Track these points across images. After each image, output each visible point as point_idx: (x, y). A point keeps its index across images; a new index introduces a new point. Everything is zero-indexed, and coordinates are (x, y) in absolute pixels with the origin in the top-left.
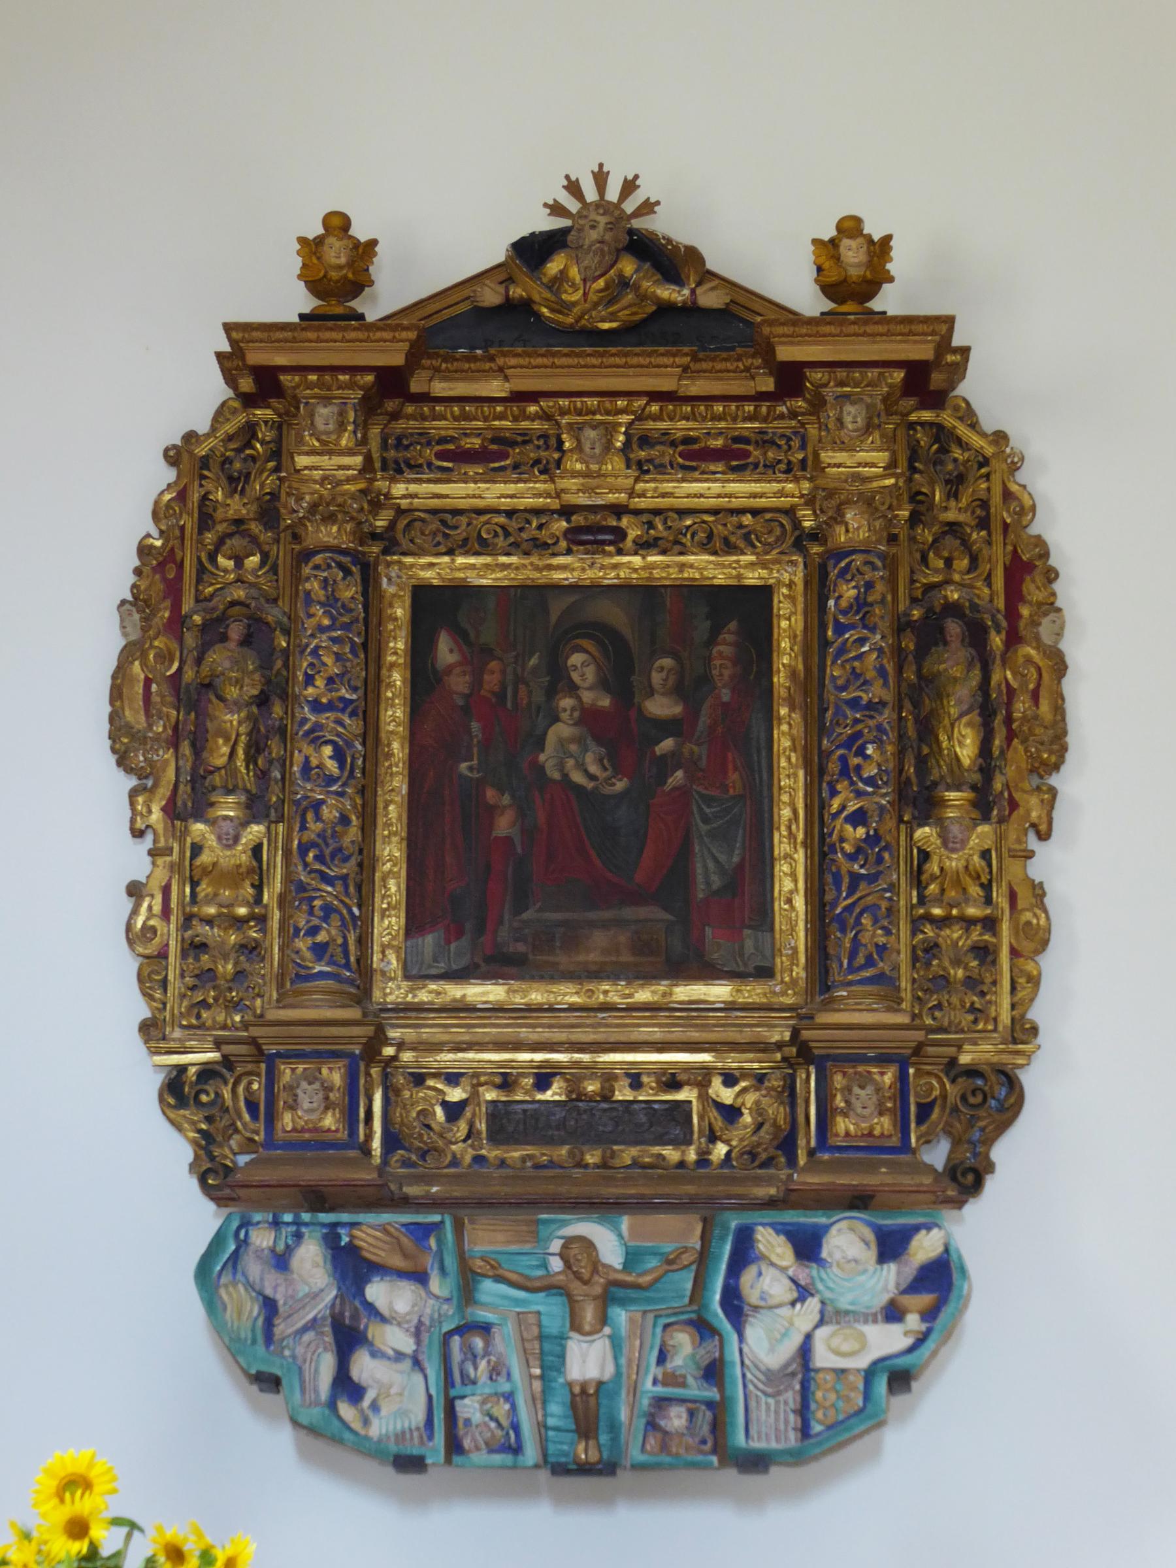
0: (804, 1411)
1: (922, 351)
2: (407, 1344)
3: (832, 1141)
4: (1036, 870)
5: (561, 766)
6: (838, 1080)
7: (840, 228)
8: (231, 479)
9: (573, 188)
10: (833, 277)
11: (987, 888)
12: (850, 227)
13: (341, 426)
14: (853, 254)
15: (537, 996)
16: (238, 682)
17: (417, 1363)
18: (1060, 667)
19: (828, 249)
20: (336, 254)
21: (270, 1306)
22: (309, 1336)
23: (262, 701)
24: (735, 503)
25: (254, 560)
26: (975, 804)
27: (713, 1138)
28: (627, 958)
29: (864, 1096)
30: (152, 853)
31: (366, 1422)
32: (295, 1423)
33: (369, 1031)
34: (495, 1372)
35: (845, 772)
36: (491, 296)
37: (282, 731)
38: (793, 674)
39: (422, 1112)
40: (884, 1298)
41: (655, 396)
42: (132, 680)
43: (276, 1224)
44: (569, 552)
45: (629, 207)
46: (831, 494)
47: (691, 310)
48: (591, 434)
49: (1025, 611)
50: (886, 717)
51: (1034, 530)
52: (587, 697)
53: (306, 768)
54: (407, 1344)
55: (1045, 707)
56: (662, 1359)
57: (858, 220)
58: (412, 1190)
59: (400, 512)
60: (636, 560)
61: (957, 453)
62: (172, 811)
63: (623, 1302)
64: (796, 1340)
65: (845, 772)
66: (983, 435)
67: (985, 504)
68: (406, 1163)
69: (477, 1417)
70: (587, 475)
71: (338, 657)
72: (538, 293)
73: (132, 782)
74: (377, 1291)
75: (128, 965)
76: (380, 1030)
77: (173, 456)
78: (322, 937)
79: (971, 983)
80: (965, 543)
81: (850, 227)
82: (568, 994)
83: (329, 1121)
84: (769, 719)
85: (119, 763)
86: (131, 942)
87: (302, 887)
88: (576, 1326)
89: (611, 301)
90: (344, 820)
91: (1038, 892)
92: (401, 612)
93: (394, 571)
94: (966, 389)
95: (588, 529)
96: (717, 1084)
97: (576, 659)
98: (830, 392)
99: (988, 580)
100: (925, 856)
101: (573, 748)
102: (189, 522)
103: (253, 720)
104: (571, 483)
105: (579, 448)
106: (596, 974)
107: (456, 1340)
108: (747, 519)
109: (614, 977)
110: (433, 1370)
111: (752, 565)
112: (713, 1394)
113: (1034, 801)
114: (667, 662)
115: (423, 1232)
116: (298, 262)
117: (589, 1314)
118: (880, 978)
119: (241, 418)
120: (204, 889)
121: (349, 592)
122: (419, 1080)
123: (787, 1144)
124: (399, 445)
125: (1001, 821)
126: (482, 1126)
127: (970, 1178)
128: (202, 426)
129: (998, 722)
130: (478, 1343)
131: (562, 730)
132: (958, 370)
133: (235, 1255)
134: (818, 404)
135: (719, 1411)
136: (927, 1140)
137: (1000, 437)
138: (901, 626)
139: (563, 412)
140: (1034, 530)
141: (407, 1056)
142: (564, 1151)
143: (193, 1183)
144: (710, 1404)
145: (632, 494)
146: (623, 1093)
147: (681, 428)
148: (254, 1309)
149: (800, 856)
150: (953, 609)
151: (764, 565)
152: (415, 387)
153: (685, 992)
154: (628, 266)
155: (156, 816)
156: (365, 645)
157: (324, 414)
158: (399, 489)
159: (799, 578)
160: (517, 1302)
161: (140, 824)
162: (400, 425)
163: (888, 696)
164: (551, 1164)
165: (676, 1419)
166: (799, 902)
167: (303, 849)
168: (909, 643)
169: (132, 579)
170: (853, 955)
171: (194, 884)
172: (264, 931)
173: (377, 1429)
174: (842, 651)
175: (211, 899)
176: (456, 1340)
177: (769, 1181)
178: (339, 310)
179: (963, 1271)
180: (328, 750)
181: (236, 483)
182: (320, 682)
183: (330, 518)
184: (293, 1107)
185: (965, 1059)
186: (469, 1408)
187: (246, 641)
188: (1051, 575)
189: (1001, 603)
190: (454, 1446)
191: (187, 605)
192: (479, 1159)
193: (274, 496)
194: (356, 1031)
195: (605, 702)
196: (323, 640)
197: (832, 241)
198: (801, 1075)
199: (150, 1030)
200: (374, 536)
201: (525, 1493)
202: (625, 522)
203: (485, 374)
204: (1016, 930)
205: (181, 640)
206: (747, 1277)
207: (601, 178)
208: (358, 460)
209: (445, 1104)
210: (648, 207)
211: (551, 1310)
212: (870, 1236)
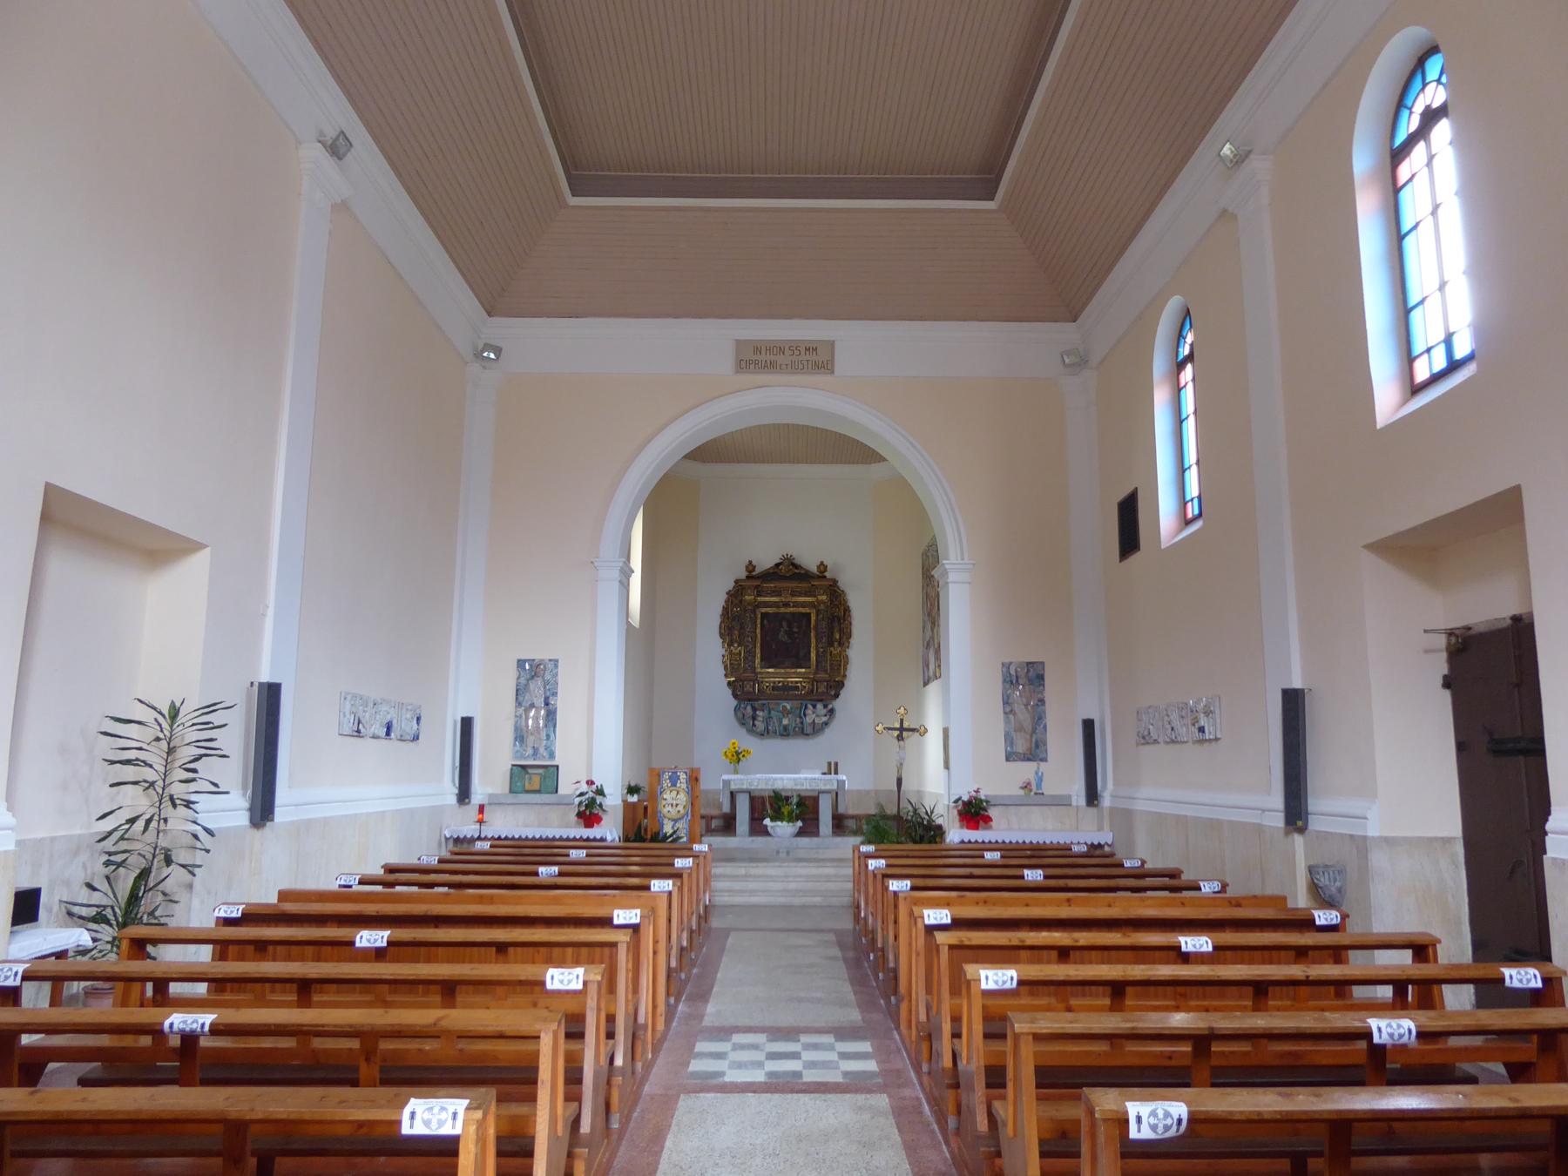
18: (851, 623)
36: (771, 571)
47: (799, 573)
77: (727, 593)
82: (783, 671)
106: (788, 668)
121: (752, 616)
123: (812, 691)
135: (803, 729)
153: (799, 670)
157: (749, 591)
165: (797, 729)
181: (736, 598)
186: (770, 728)
188: (850, 611)
190: (768, 733)
199: (726, 676)
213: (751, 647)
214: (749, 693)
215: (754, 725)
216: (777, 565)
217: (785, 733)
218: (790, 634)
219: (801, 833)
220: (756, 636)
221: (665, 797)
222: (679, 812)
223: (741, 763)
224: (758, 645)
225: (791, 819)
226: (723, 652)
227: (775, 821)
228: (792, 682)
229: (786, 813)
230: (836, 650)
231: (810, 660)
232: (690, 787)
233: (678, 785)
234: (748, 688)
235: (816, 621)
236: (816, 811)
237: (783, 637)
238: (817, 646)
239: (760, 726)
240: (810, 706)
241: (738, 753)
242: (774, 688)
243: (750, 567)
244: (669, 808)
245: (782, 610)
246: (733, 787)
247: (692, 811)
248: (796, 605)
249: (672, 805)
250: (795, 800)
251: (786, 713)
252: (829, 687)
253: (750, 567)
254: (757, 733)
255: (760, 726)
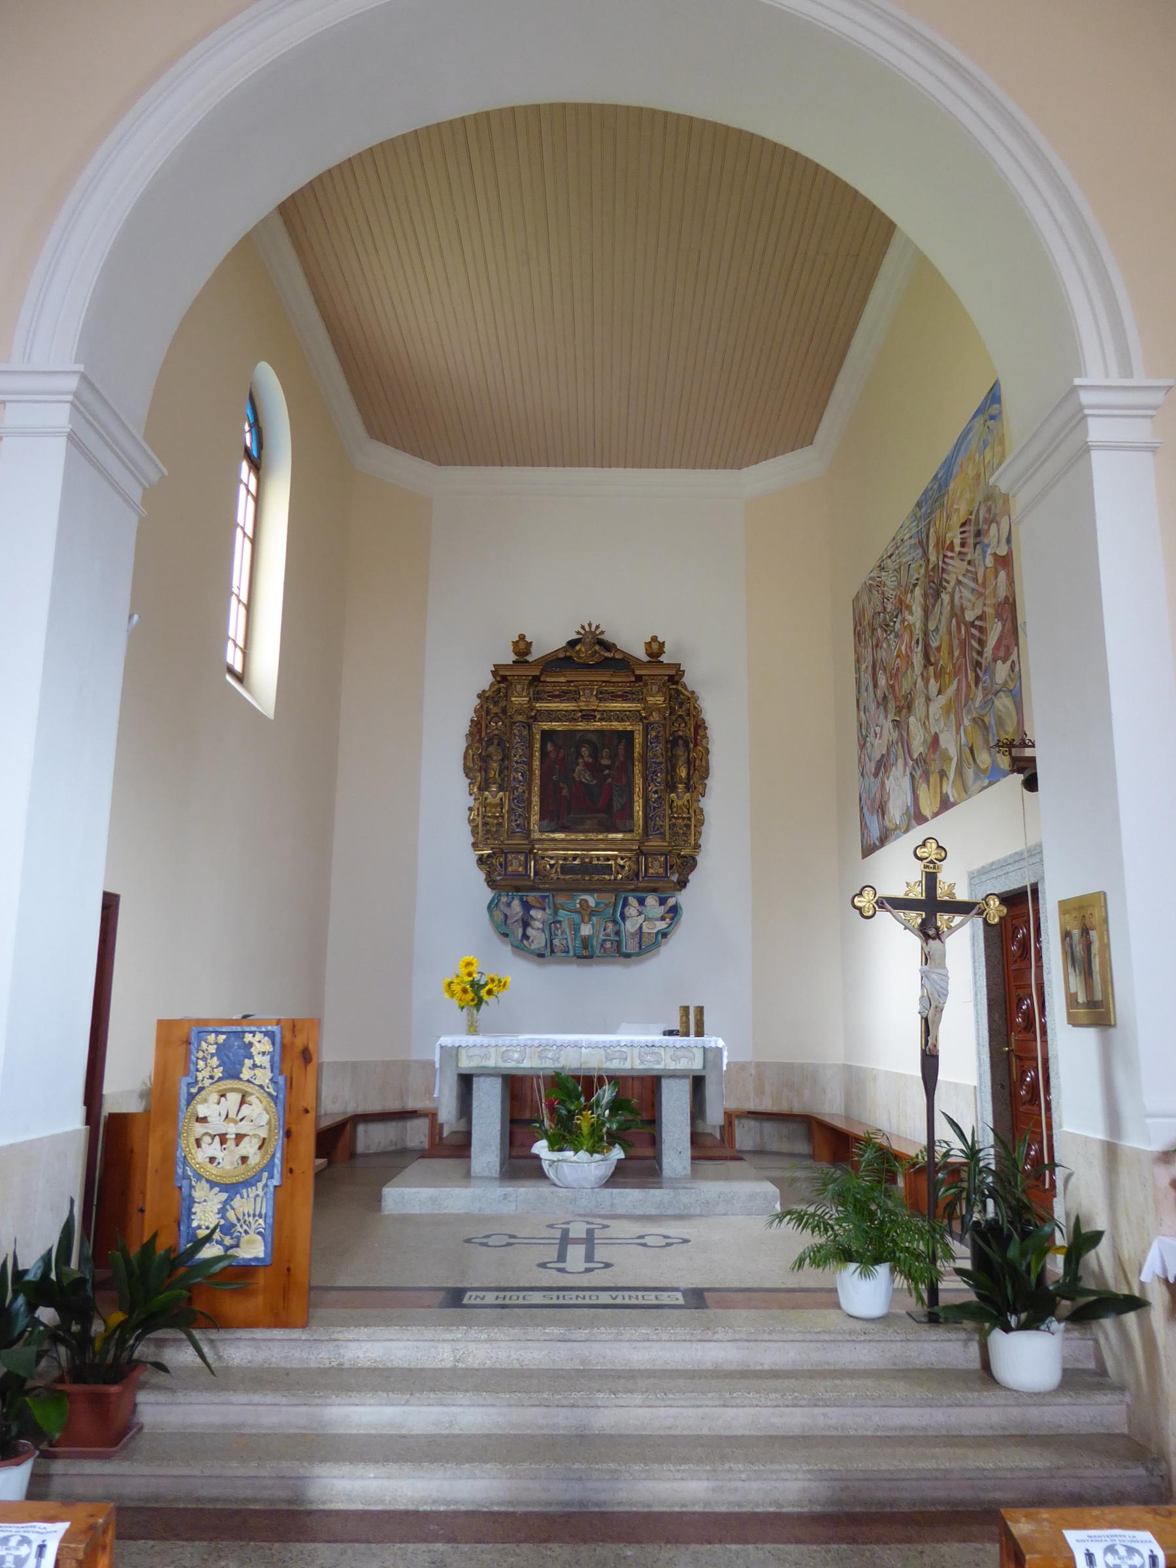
0: (640, 943)
1: (673, 672)
2: (541, 926)
3: (649, 875)
4: (701, 805)
5: (579, 777)
6: (650, 859)
7: (652, 639)
8: (495, 703)
9: (583, 627)
10: (650, 652)
11: (688, 810)
12: (654, 639)
13: (523, 690)
14: (655, 646)
15: (573, 837)
16: (496, 755)
17: (543, 931)
18: (707, 751)
19: (648, 645)
20: (522, 645)
21: (506, 916)
22: (516, 924)
23: (502, 760)
24: (625, 709)
25: (501, 723)
26: (686, 788)
27: (618, 873)
28: (596, 827)
29: (656, 863)
30: (475, 799)
31: (530, 945)
32: (512, 945)
33: (530, 846)
34: (562, 933)
35: (652, 780)
36: (561, 655)
37: (507, 768)
38: (639, 753)
39: (544, 867)
40: (661, 915)
41: (604, 682)
42: (469, 755)
43: (507, 895)
44: (581, 721)
45: (597, 632)
46: (649, 708)
47: (613, 659)
48: (587, 691)
49: (699, 737)
50: (663, 766)
51: (701, 717)
52: (586, 759)
53: (514, 778)
54: (541, 926)
55: (704, 762)
56: (605, 930)
57: (657, 637)
58: (541, 886)
59: (538, 711)
60: (599, 724)
61: (682, 696)
62: (479, 789)
63: (594, 915)
64: (639, 925)
65: (652, 780)
66: (688, 691)
67: (689, 710)
68: (540, 879)
69: (558, 944)
70: (586, 702)
71: (523, 750)
72: (574, 655)
73: (469, 781)
74: (533, 913)
75: (469, 828)
76: (533, 846)
77: (479, 696)
78: (518, 822)
79: (684, 834)
80: (683, 719)
81: (654, 639)
82: (581, 837)
83: (520, 869)
84: (633, 765)
85: (466, 776)
86: (469, 822)
87: (513, 809)
88: (583, 921)
89: (593, 656)
90: (524, 792)
91: (701, 810)
92: (538, 737)
93: (536, 726)
94: (684, 680)
95: (587, 715)
96: (619, 859)
97: (584, 749)
98: (649, 682)
99: (690, 730)
100: (673, 801)
101: (583, 772)
102: (484, 713)
103: (500, 765)
104: (582, 704)
105: (584, 695)
106: (588, 831)
107: (553, 925)
108: (628, 713)
109: (593, 832)
110: (547, 932)
111: (628, 725)
112: (617, 939)
113: (700, 787)
114: (607, 750)
115: (544, 897)
116: (512, 647)
117: (586, 918)
118: (661, 833)
119: (497, 687)
120: (488, 809)
121: (525, 733)
122: (543, 858)
123: (637, 875)
124: (537, 694)
125: (692, 792)
126: (559, 870)
127: (683, 884)
128: (487, 688)
129: (692, 766)
130: (558, 925)
131: (580, 768)
132: (682, 675)
133: (497, 903)
134: (646, 685)
135: (619, 943)
136: (672, 874)
137: (693, 692)
138: (667, 742)
139: (580, 685)
140: (701, 717)
141: (540, 852)
142: (580, 876)
143: (486, 884)
144: (616, 941)
145: (598, 706)
146: (595, 862)
147: (610, 689)
148: (502, 917)
149: (641, 801)
150: (680, 737)
151: (632, 725)
152: (542, 679)
153: (611, 836)
154: (597, 648)
155: (476, 790)
156: (529, 747)
157: (519, 687)
158: (538, 705)
159: (641, 729)
160: (568, 915)
161: (471, 792)
162: (538, 688)
163: (663, 760)
164: (576, 880)
165: (608, 945)
166: (641, 813)
167: (514, 799)
168: (669, 746)
169: (469, 728)
170: (654, 828)
171: (485, 807)
172: (503, 819)
173: (533, 947)
174: (652, 748)
175: (489, 812)
176: (553, 925)
177: (632, 884)
178: (522, 660)
179: (681, 908)
180: (520, 774)
181: (496, 703)
182: (518, 756)
183: (520, 714)
184: (511, 866)
185: (682, 853)
186: (556, 942)
187: (498, 745)
188: (706, 728)
189: (693, 735)
190: (552, 951)
191: (483, 734)
192: (558, 878)
193: (505, 707)
194: (526, 846)
195: (591, 760)
196: (518, 745)
197: (650, 642)
198: (641, 857)
199: (475, 845)
200: (532, 717)
201: (569, 963)
202: (596, 714)
203: (560, 676)
204: (695, 820)
205: (482, 744)
206: (626, 910)
207: (590, 625)
208: (527, 699)
209: (550, 865)
210: (602, 633)
211: (576, 918)
212: (657, 899)
213: (520, 790)
214: (516, 875)
215: (525, 936)
216: (572, 644)
217: (584, 953)
218: (594, 768)
219: (619, 1176)
220: (531, 770)
221: (202, 1111)
222: (244, 1159)
223: (484, 1006)
224: (536, 789)
225: (598, 1143)
226: (470, 802)
227: (561, 1150)
228: (598, 858)
229: (585, 1129)
230: (680, 798)
231: (631, 816)
232: (281, 1080)
233: (246, 1074)
234: (515, 866)
235: (645, 746)
236: (653, 1121)
237: (581, 774)
238: (645, 789)
239: (538, 938)
240: (632, 901)
241: (476, 986)
242: (565, 870)
243: (522, 647)
244: (214, 1149)
245: (582, 726)
246: (466, 1064)
247: (285, 1159)
248: (607, 716)
249: (223, 1139)
250: (606, 1094)
251: (587, 913)
252: (668, 867)
253: (522, 647)
254: (531, 952)
255: (538, 938)
